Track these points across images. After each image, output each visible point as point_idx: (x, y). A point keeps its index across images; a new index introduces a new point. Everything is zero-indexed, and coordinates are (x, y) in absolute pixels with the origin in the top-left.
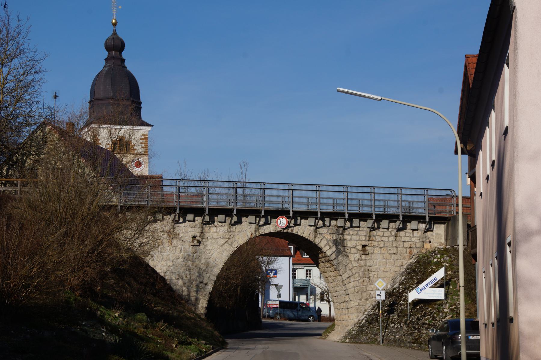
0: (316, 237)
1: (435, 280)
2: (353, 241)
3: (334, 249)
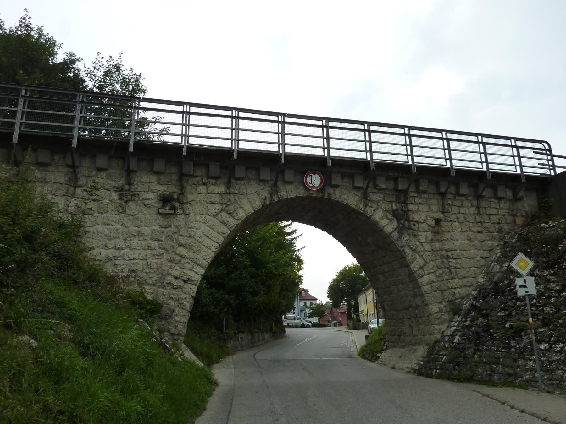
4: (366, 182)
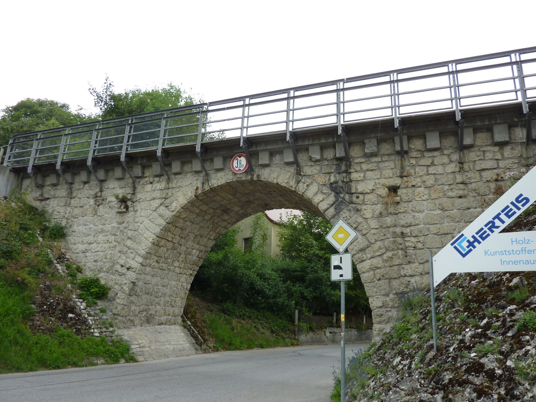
0: (298, 183)
1: (519, 205)
2: (369, 182)
3: (332, 199)
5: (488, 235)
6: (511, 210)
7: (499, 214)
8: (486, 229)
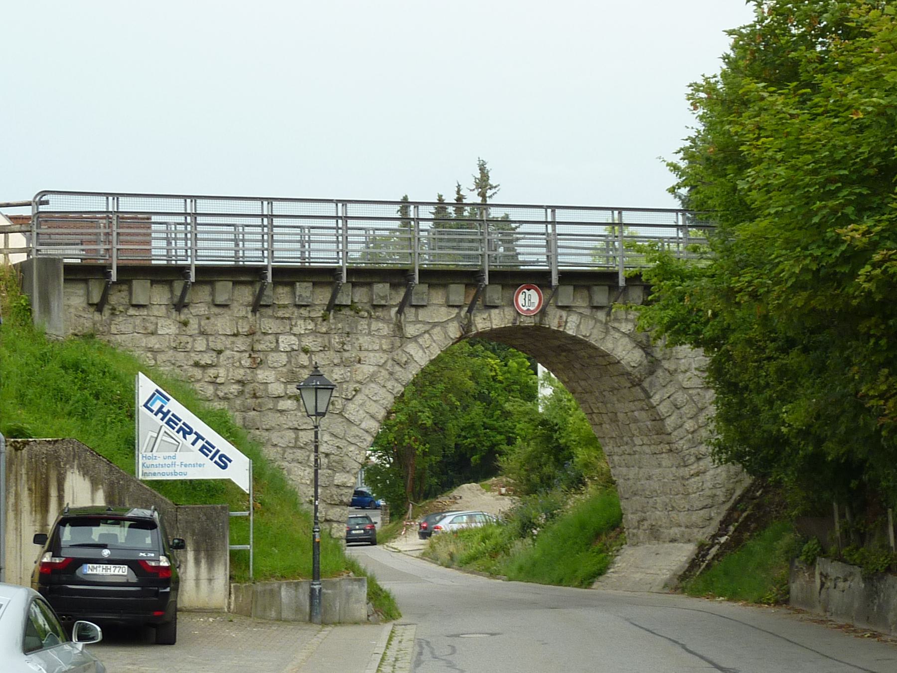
4: (473, 292)
5: (207, 455)
6: (210, 452)
7: (203, 439)
8: (180, 424)
